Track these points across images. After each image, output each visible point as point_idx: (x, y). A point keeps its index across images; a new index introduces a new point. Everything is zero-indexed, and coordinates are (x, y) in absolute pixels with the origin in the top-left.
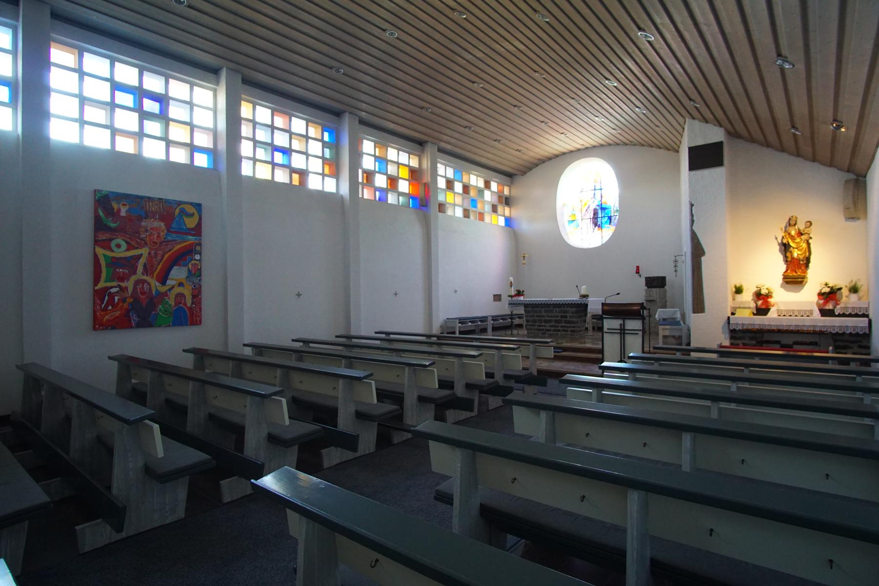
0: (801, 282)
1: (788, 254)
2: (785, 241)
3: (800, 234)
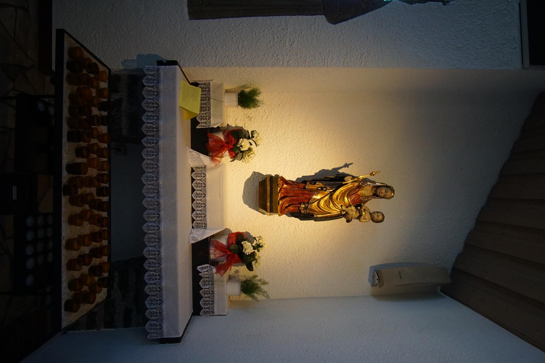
1: (319, 185)
2: (349, 180)
3: (358, 204)
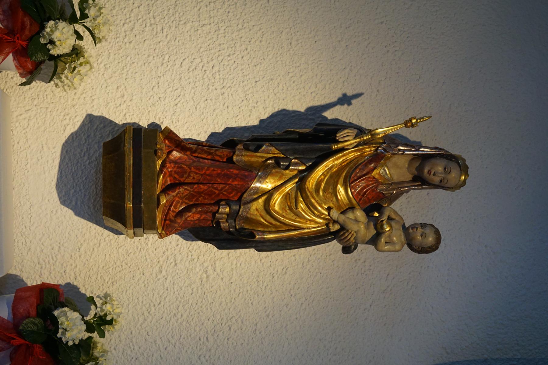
0: (120, 217)
1: (269, 152)
2: (347, 138)
3: (374, 205)
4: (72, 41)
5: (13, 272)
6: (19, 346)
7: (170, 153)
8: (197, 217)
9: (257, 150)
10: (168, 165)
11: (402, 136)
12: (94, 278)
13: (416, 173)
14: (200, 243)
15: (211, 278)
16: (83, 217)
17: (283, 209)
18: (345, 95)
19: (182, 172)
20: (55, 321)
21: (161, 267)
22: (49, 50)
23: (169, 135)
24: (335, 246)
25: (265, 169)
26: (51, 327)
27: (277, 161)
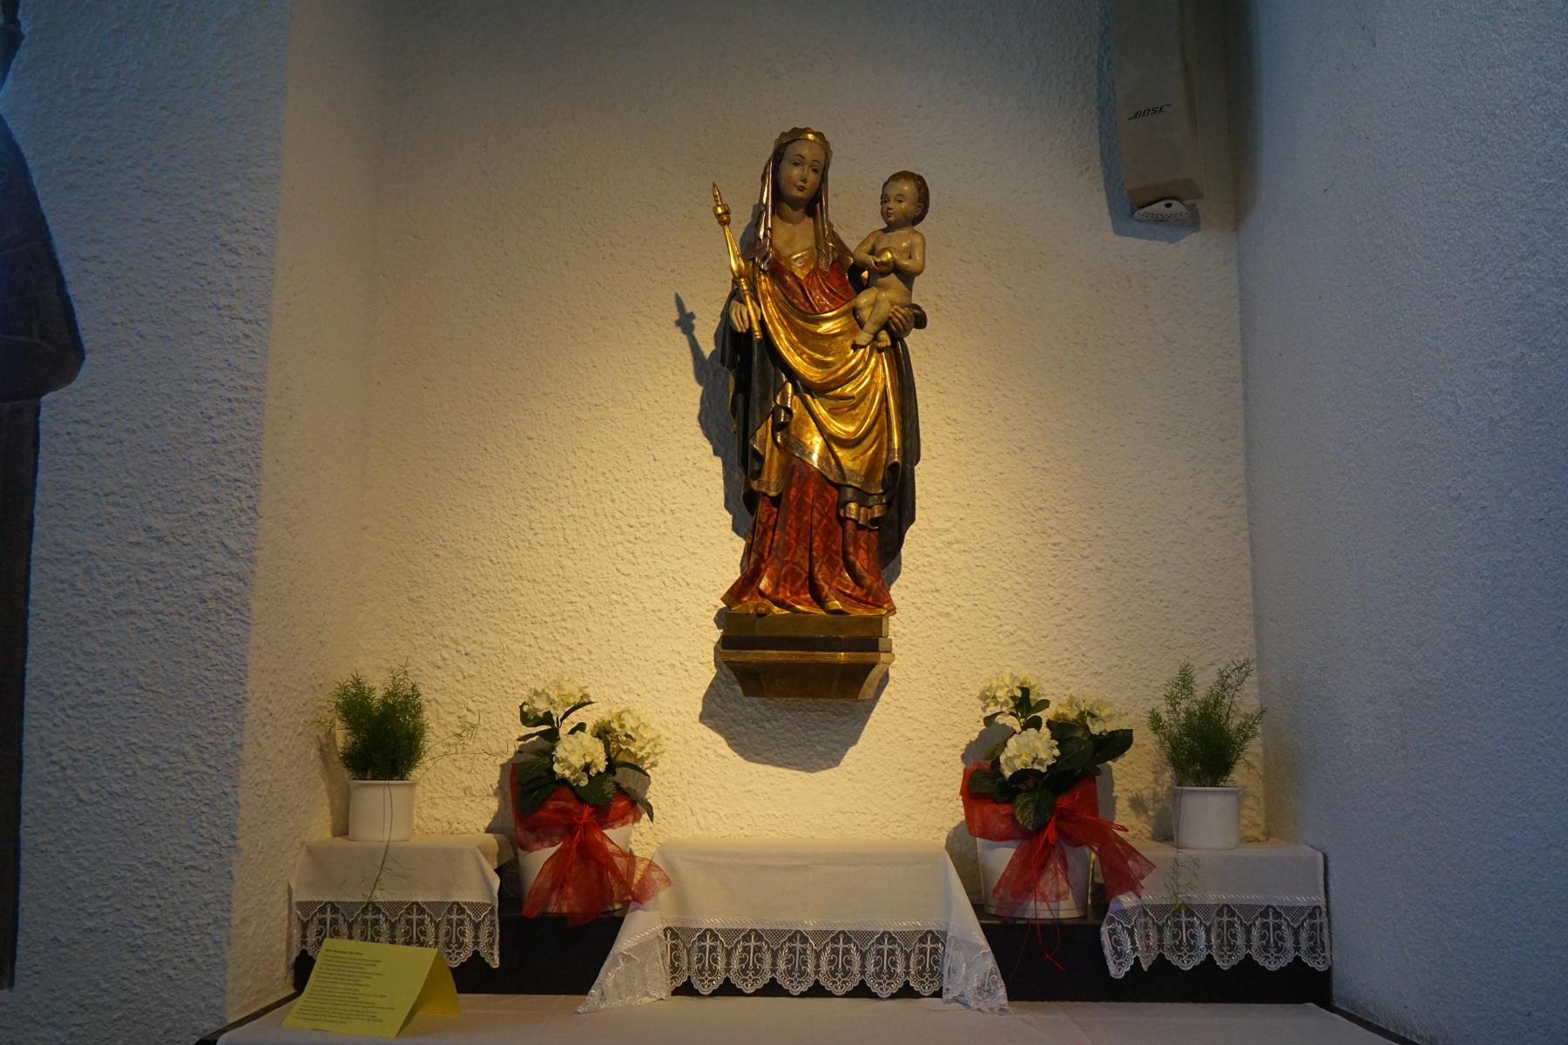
1: (764, 439)
2: (747, 314)
3: (851, 276)
4: (586, 738)
5: (943, 841)
6: (1060, 831)
7: (762, 594)
8: (862, 554)
9: (760, 458)
10: (781, 596)
11: (744, 235)
12: (955, 718)
13: (802, 210)
14: (904, 551)
15: (960, 537)
16: (860, 732)
17: (853, 419)
18: (678, 323)
19: (793, 576)
20: (1022, 775)
21: (940, 614)
22: (599, 773)
23: (735, 594)
24: (913, 340)
25: (792, 448)
26: (1030, 783)
27: (778, 427)
